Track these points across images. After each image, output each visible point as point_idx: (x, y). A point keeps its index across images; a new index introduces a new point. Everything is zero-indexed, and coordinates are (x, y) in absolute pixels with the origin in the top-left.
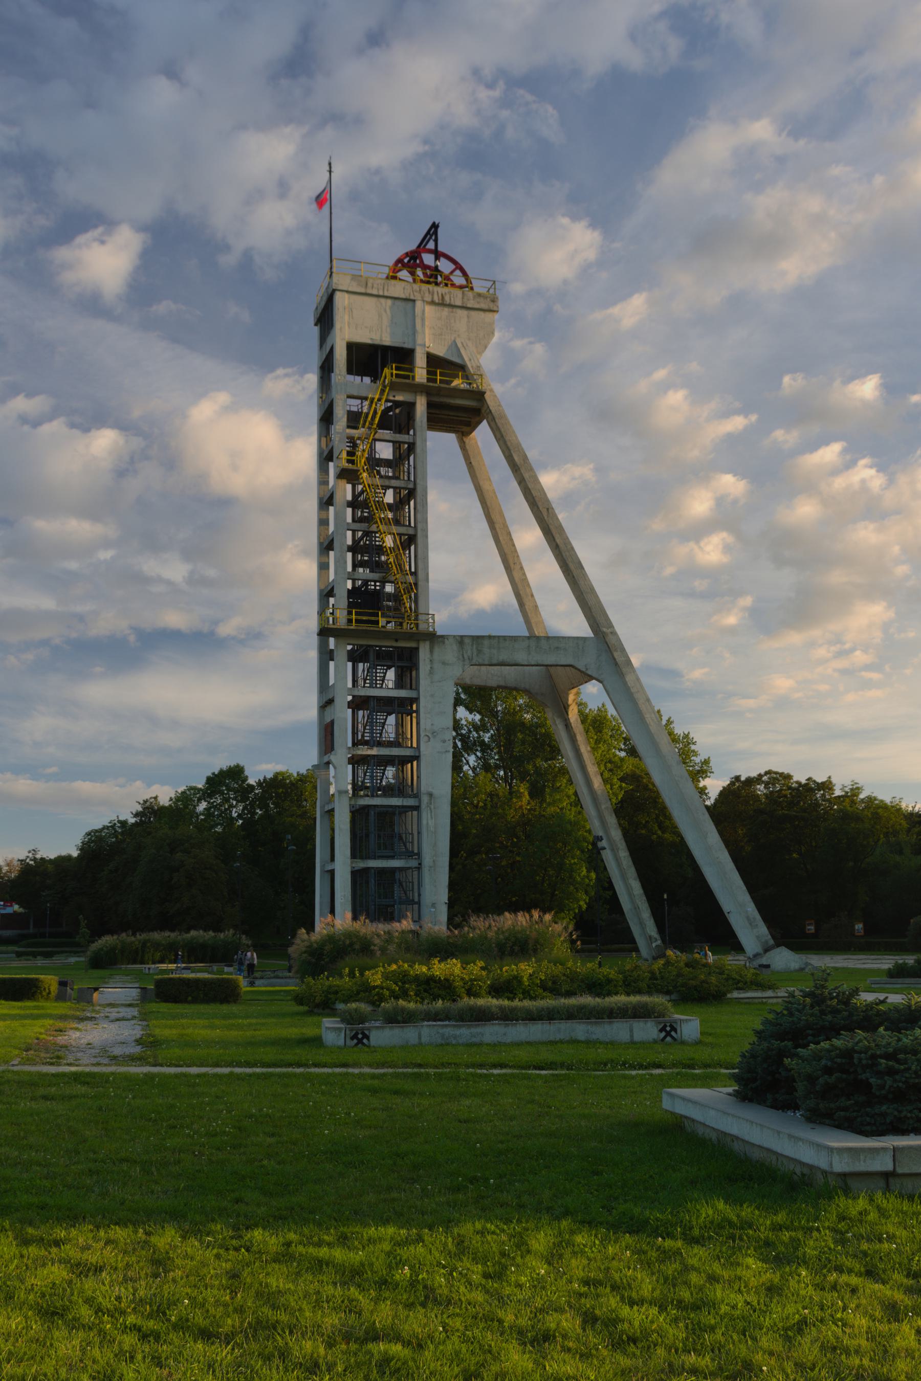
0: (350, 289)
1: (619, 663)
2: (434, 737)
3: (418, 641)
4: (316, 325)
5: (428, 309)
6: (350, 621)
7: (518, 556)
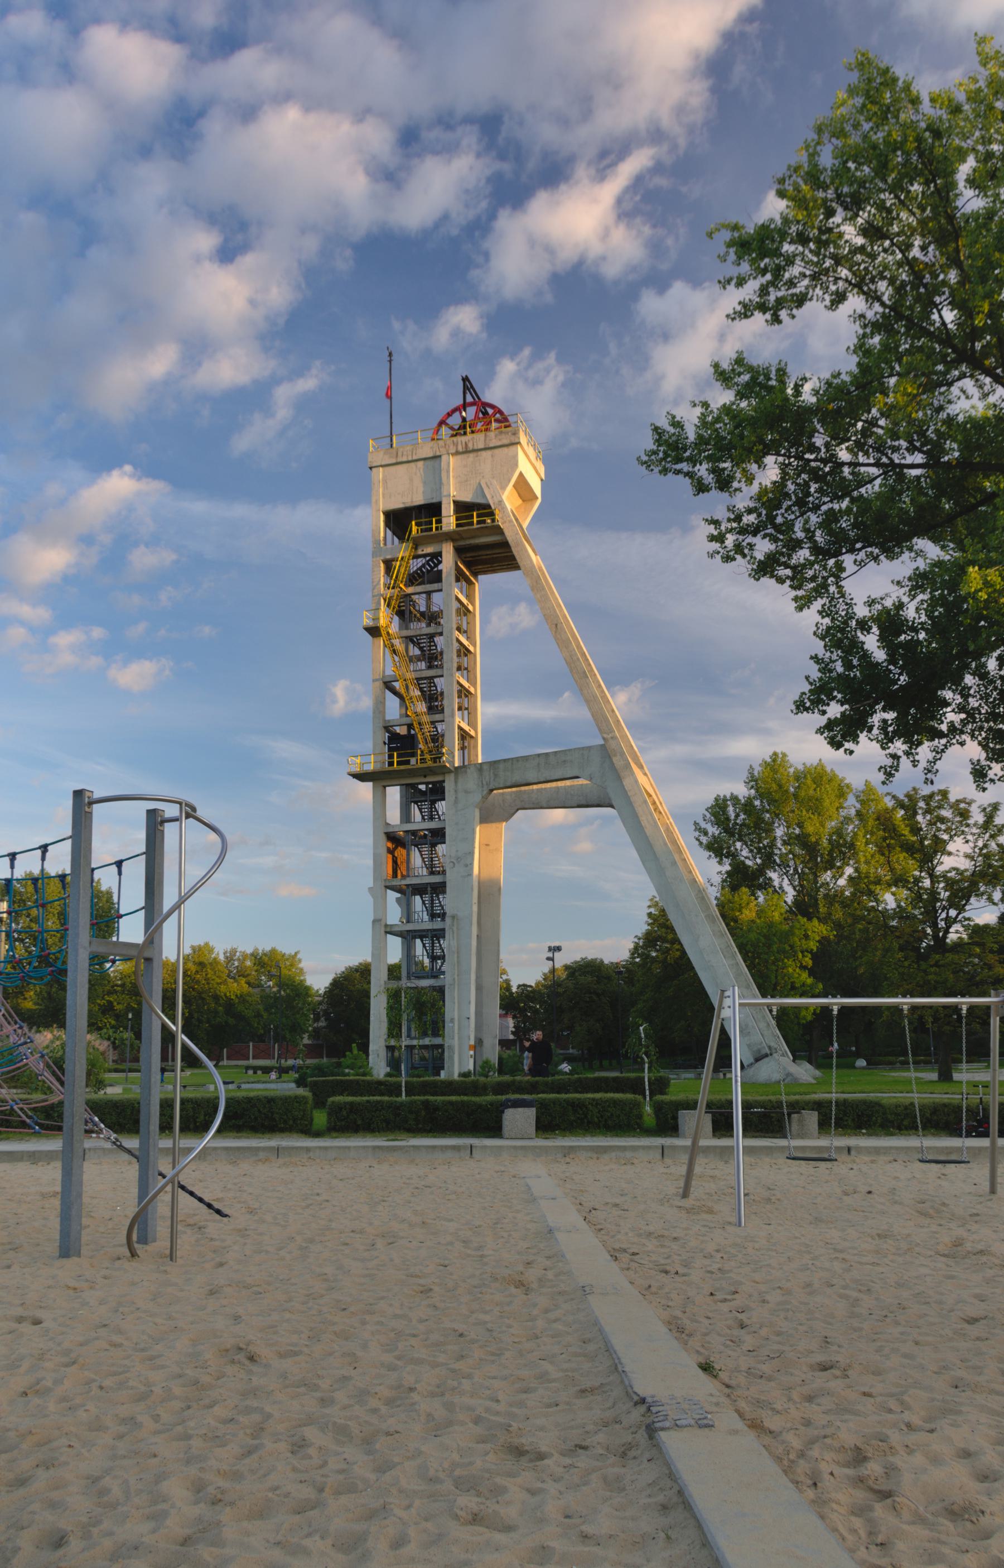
1: (618, 767)
6: (391, 764)
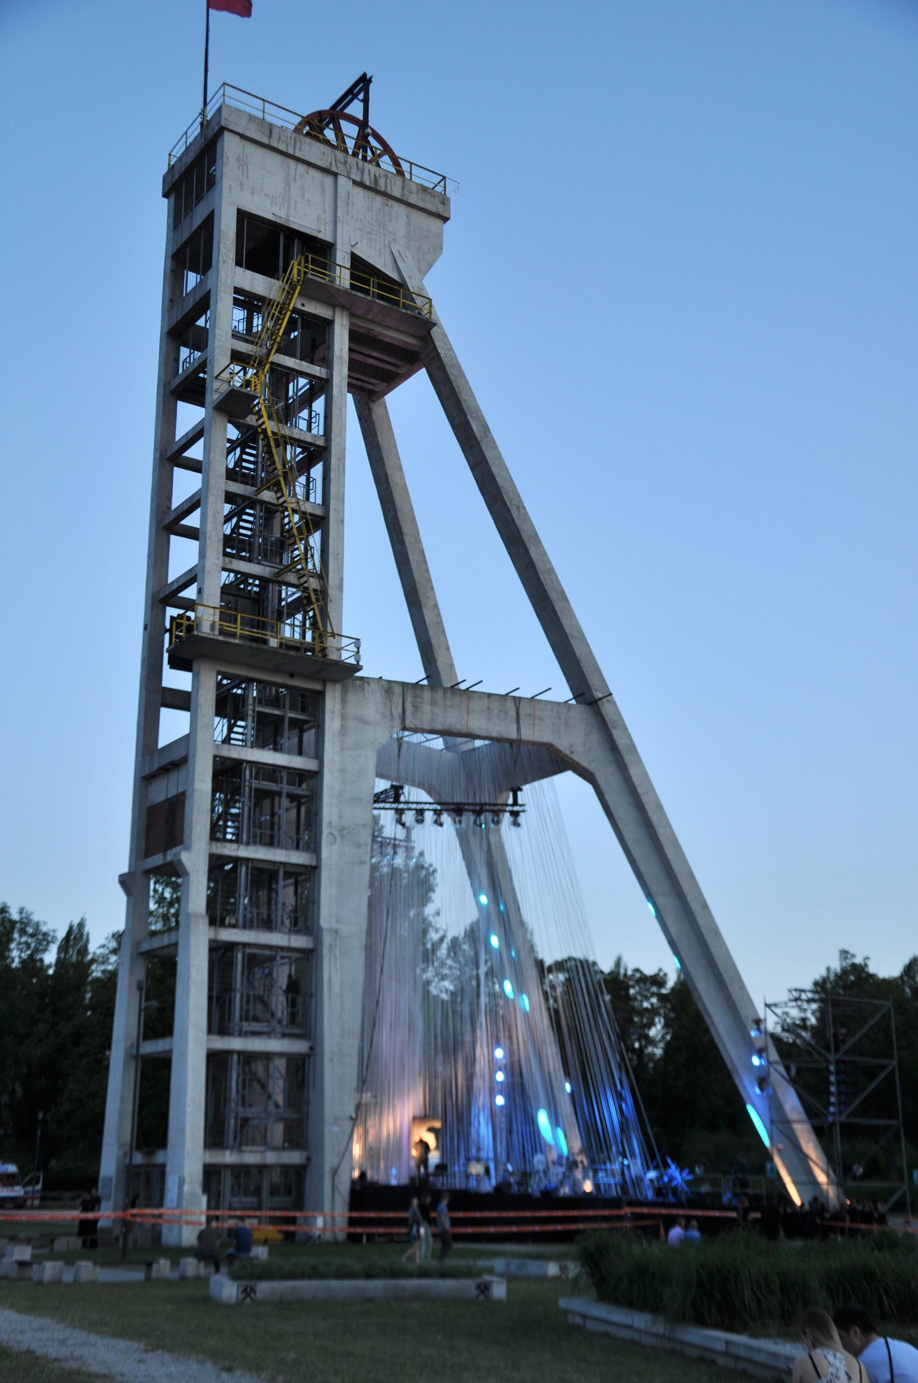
0: (247, 134)
1: (620, 747)
2: (343, 837)
3: (324, 682)
4: (166, 195)
5: (359, 192)
7: (432, 588)
